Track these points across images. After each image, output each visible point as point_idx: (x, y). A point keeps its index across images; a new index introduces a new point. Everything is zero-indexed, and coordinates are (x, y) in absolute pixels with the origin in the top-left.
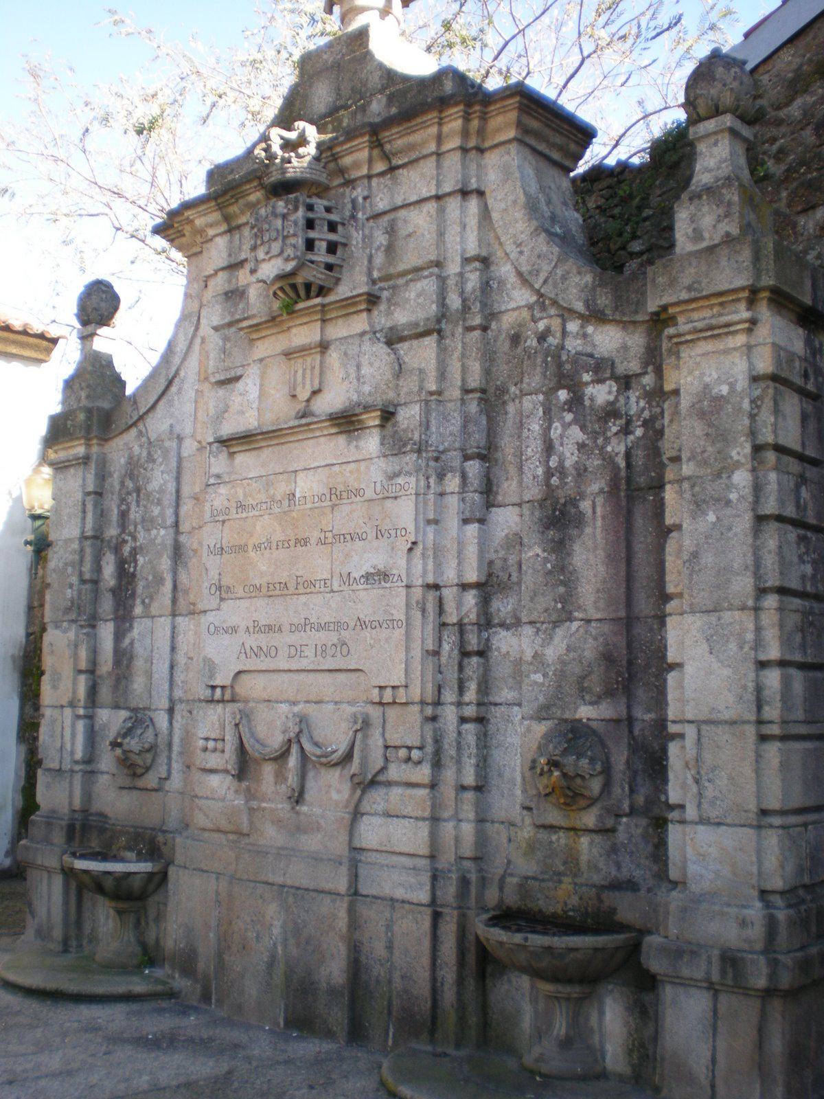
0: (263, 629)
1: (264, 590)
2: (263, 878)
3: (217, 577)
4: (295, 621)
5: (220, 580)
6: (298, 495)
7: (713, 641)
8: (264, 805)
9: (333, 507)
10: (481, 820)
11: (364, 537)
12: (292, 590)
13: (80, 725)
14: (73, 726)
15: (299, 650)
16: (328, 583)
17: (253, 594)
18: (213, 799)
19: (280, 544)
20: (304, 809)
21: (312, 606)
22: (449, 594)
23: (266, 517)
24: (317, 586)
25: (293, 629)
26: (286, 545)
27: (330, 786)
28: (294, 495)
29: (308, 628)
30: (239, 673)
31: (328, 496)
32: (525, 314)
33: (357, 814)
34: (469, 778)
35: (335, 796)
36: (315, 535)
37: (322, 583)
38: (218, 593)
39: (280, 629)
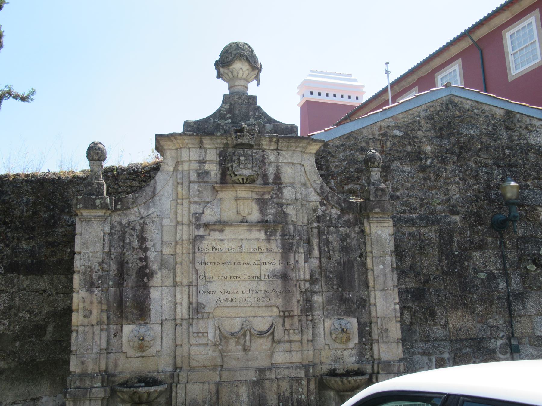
0: (229, 292)
1: (229, 279)
2: (235, 379)
3: (203, 273)
4: (245, 290)
5: (205, 274)
6: (243, 248)
7: (386, 299)
8: (229, 354)
9: (260, 253)
10: (314, 350)
11: (274, 263)
12: (242, 278)
13: (104, 334)
14: (100, 334)
15: (247, 300)
16: (260, 277)
17: (223, 280)
18: (202, 355)
19: (236, 264)
20: (250, 353)
21: (252, 285)
22: (302, 283)
23: (228, 253)
24: (254, 278)
25: (244, 292)
26: (239, 264)
27: (262, 344)
28: (242, 247)
29: (251, 292)
30: (217, 307)
31: (258, 249)
32: (318, 204)
33: (273, 353)
34: (310, 338)
35: (264, 347)
36: (252, 262)
37: (257, 277)
38: (204, 279)
39: (237, 292)
